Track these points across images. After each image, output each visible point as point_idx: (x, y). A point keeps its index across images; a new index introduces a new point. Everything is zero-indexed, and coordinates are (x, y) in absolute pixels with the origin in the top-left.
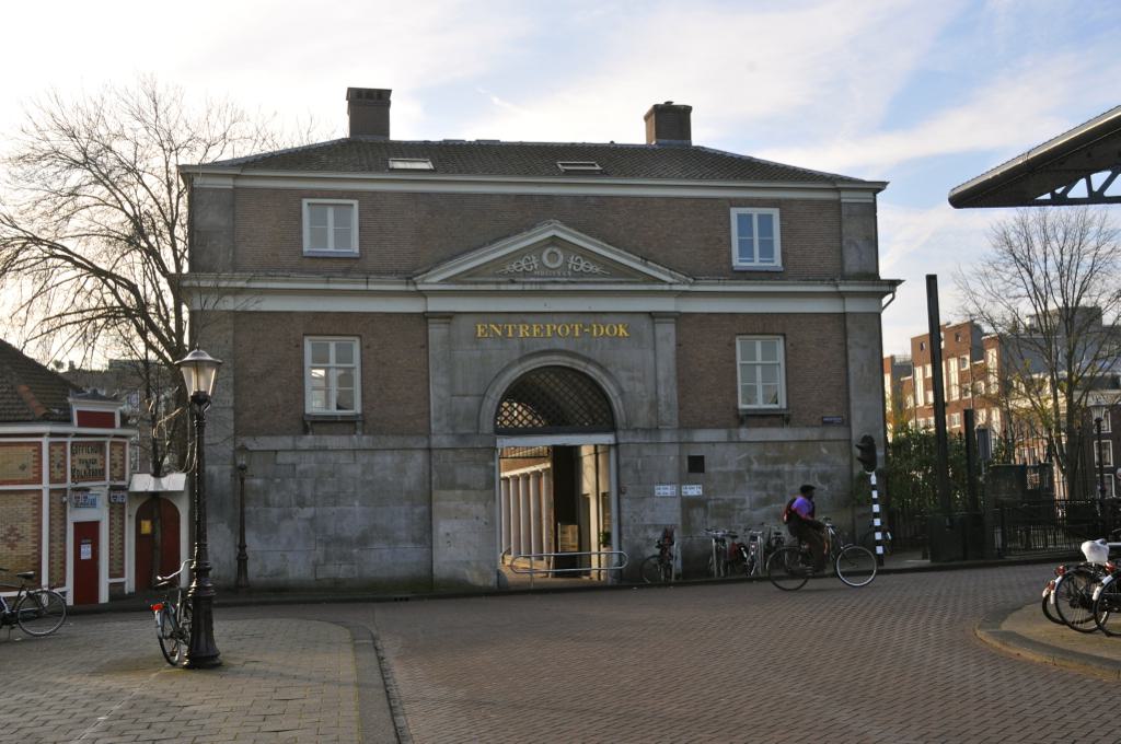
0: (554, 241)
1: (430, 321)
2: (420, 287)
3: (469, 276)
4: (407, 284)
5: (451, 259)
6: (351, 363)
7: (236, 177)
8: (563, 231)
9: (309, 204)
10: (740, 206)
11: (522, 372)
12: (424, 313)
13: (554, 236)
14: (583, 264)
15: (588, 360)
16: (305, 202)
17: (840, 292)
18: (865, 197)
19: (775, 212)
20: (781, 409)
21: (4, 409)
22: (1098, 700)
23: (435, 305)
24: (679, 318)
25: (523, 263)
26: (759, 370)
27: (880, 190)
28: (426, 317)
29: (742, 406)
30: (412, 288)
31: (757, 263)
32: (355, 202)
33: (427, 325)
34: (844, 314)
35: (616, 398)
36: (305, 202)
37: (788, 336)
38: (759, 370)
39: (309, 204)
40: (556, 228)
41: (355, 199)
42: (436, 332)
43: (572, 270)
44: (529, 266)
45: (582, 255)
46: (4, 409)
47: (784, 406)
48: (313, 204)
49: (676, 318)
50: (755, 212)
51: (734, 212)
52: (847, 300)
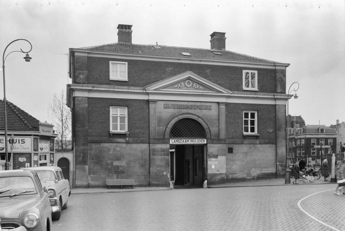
0: (189, 78)
1: (150, 102)
2: (147, 91)
3: (162, 88)
4: (143, 90)
5: (210, 86)
6: (254, 118)
7: (88, 53)
8: (192, 75)
9: (112, 63)
10: (246, 69)
11: (196, 120)
12: (148, 100)
13: (190, 77)
14: (198, 86)
15: (199, 117)
16: (110, 62)
17: (275, 98)
18: (284, 68)
19: (256, 72)
20: (256, 134)
21: (1, 124)
22: (286, 224)
23: (152, 97)
24: (227, 104)
25: (179, 85)
26: (119, 118)
27: (287, 66)
28: (148, 101)
29: (112, 130)
30: (144, 91)
31: (250, 88)
32: (127, 63)
33: (149, 104)
34: (276, 105)
35: (206, 129)
36: (110, 62)
37: (258, 111)
38: (119, 118)
39: (112, 63)
40: (190, 74)
41: (242, 72)
42: (152, 106)
43: (194, 88)
44: (181, 86)
45: (198, 83)
46: (1, 124)
47: (127, 131)
48: (113, 63)
49: (226, 104)
50: (250, 72)
51: (244, 72)
52: (277, 101)
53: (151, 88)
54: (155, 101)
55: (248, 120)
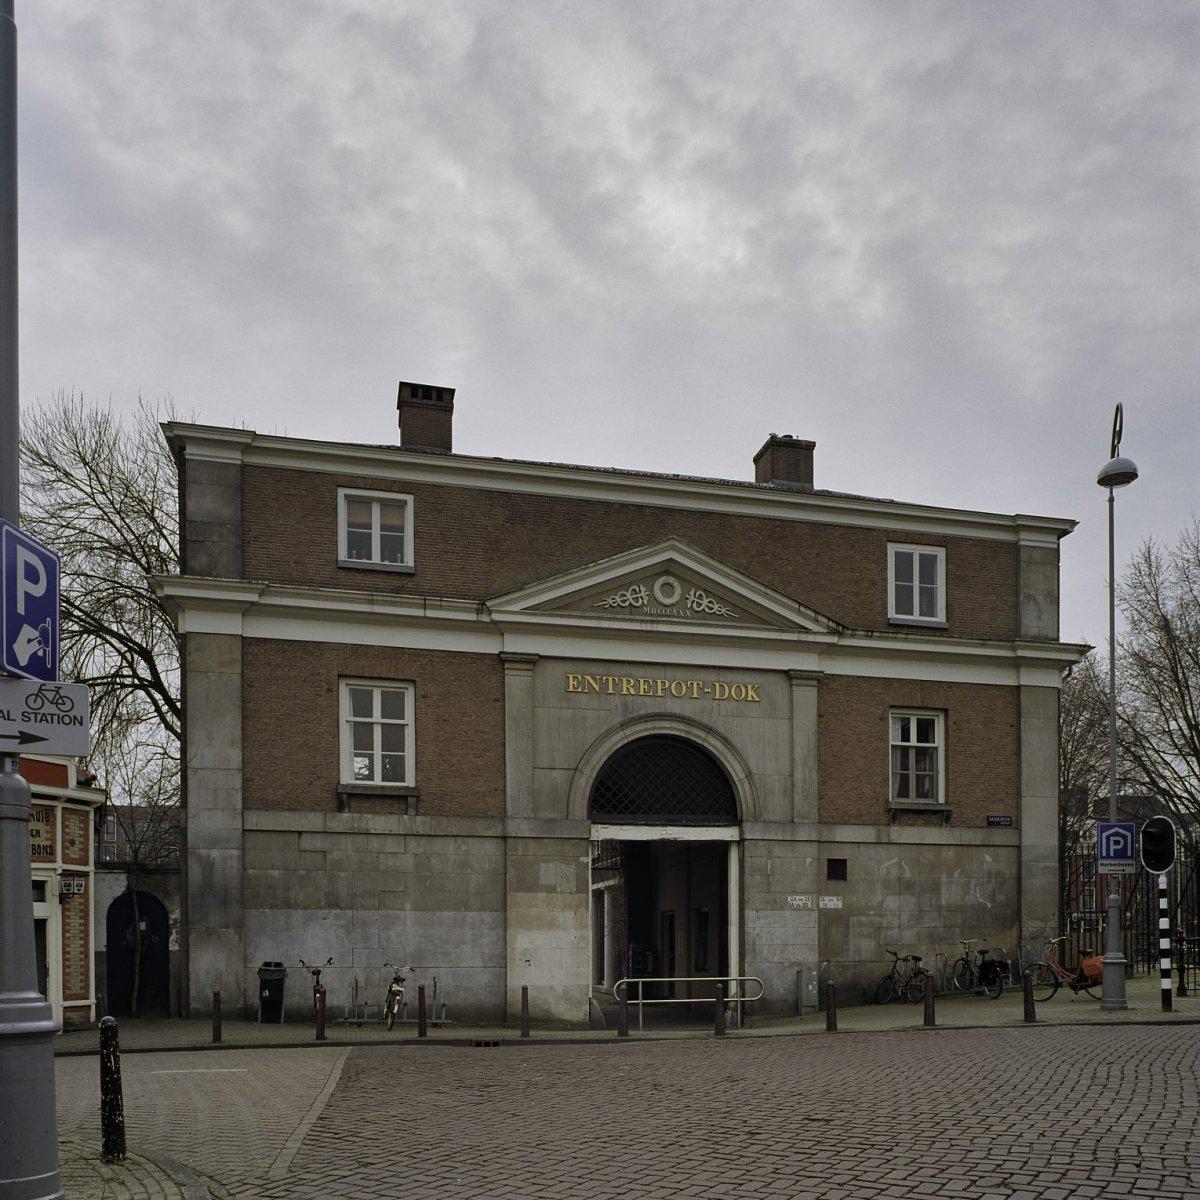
28: (501, 660)
53: (511, 609)
54: (532, 661)
55: (371, 724)
